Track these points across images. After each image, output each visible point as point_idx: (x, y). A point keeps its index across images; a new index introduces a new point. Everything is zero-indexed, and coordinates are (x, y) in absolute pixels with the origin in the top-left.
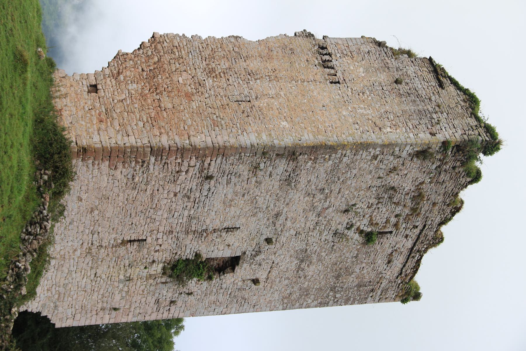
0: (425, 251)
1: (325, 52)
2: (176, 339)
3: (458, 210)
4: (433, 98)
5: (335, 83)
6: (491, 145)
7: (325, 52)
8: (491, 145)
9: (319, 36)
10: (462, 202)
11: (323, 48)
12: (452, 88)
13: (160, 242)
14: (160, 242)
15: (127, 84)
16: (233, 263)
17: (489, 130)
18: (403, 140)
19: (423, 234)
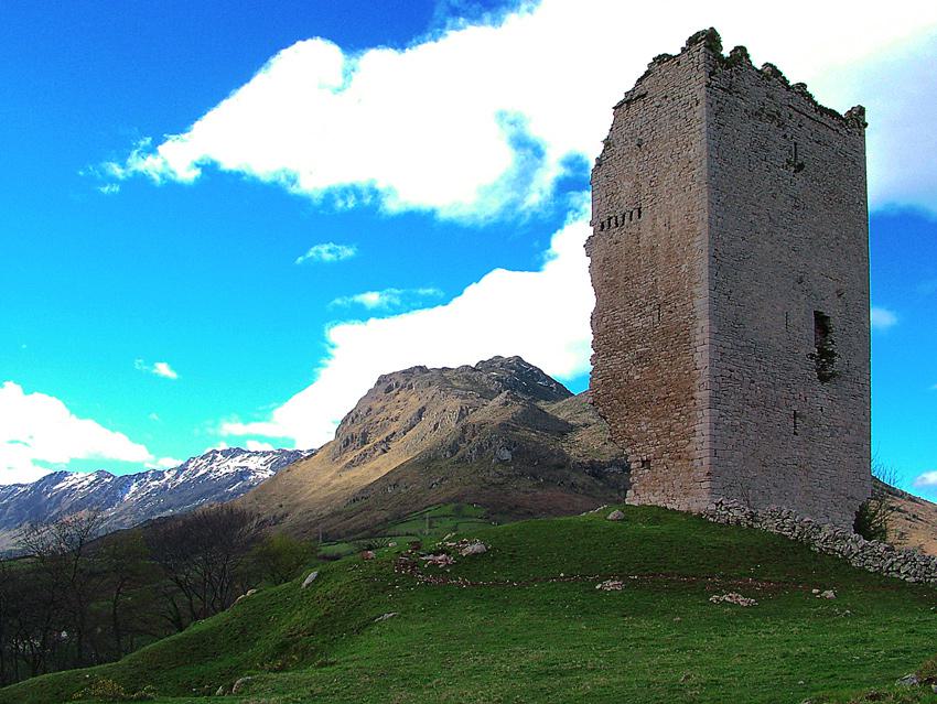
0: (815, 103)
1: (606, 224)
2: (332, 437)
3: (776, 72)
4: (657, 104)
5: (640, 212)
6: (710, 39)
7: (606, 224)
8: (710, 39)
9: (590, 232)
10: (767, 65)
11: (603, 227)
12: (646, 83)
13: (797, 396)
14: (797, 396)
15: (642, 431)
16: (821, 322)
17: (692, 41)
18: (704, 135)
19: (797, 107)
